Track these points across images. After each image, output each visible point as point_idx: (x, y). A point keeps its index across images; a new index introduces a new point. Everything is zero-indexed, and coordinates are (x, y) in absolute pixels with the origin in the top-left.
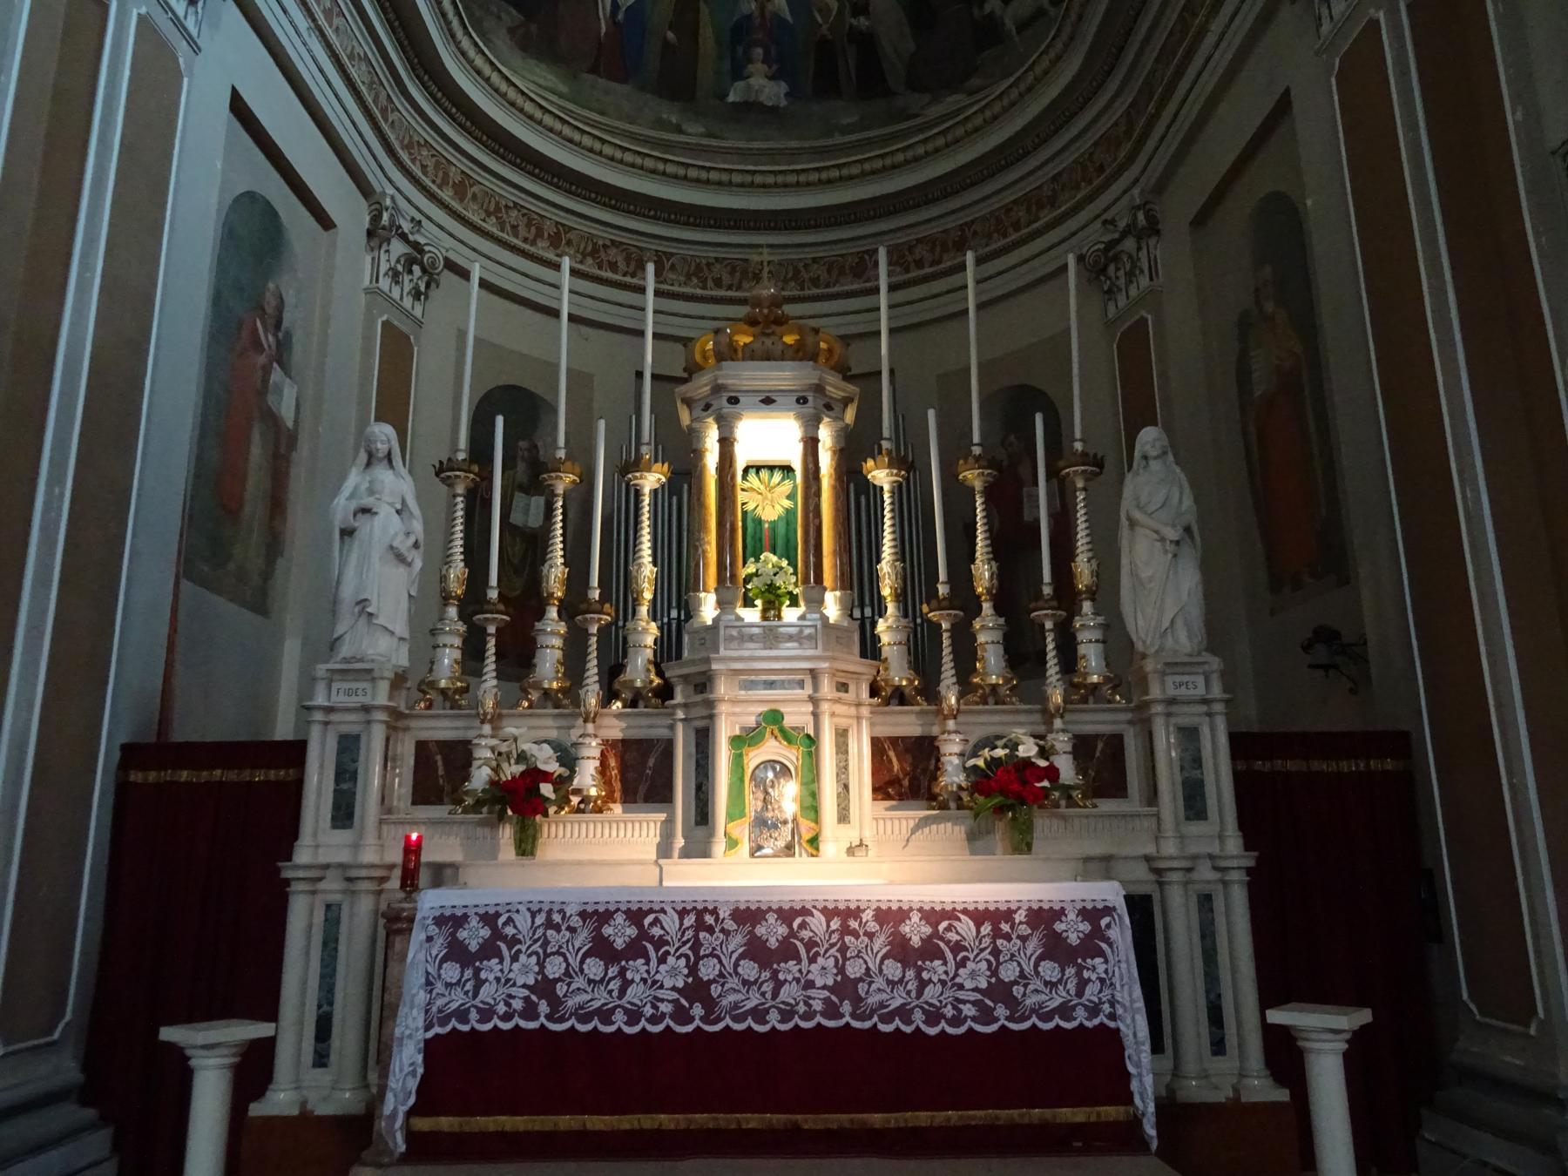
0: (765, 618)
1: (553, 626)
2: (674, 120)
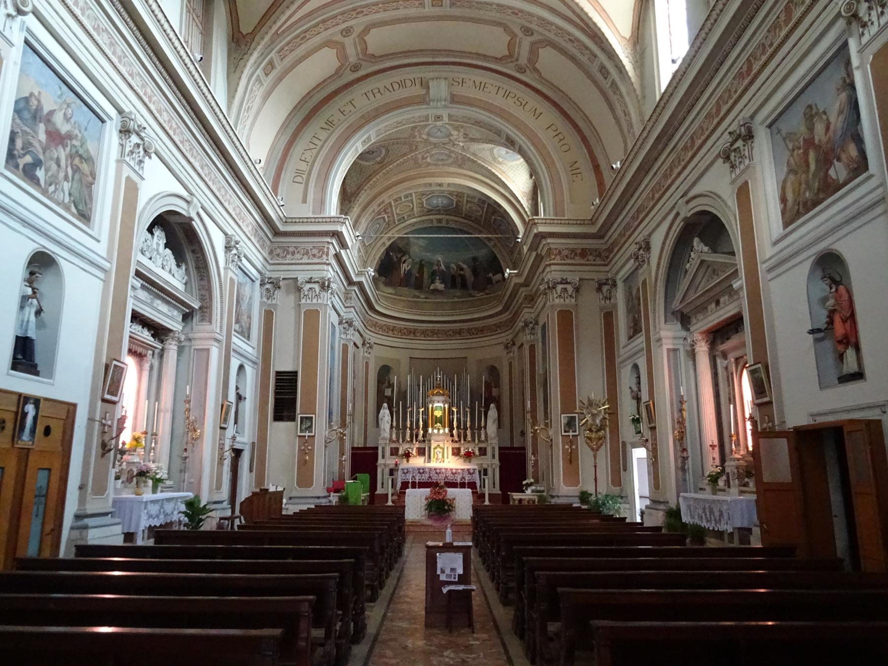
1: (408, 431)
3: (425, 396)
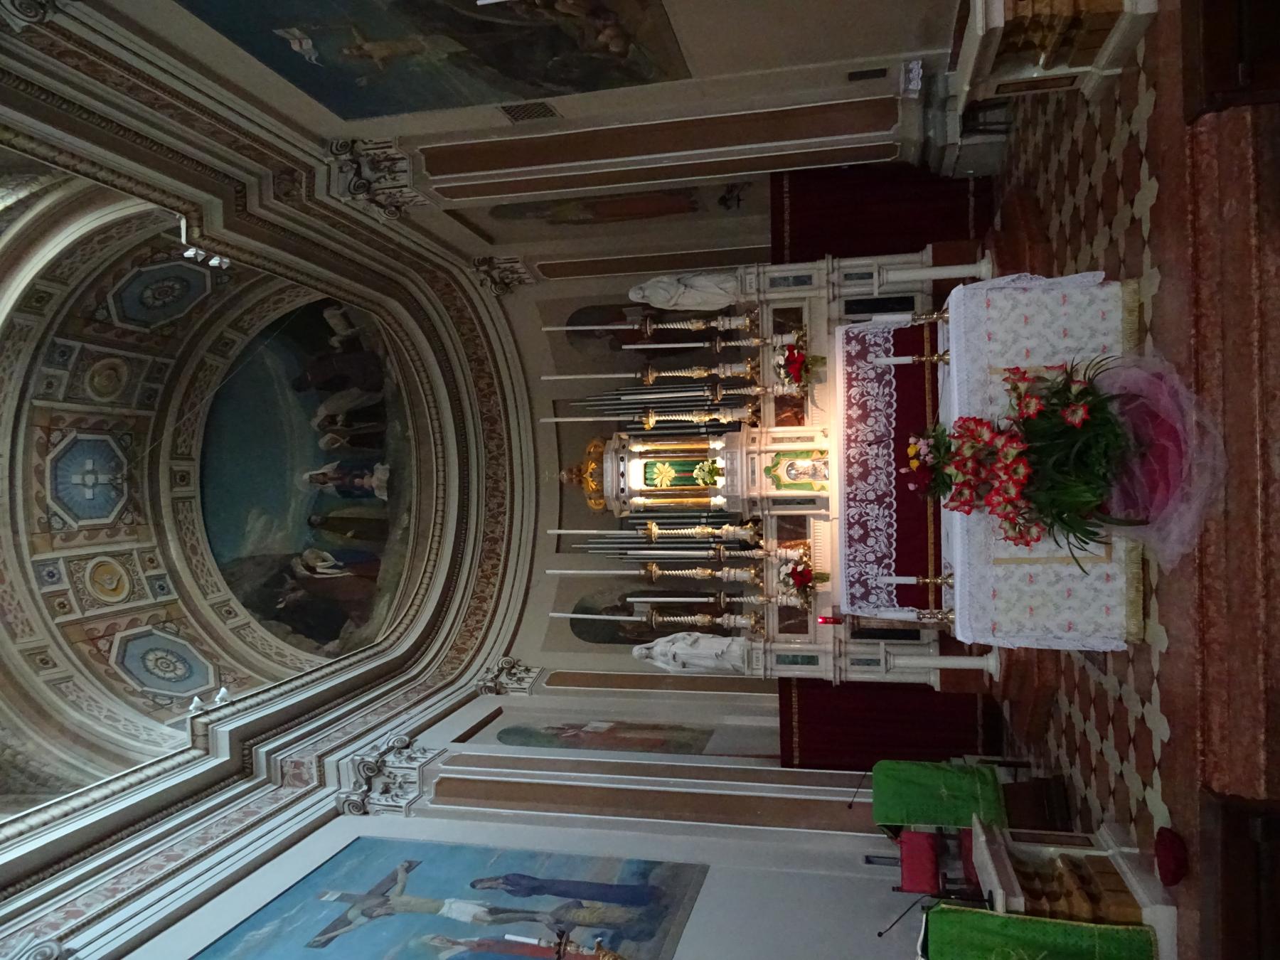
0: (723, 475)
1: (726, 573)
2: (400, 532)
3: (606, 518)
